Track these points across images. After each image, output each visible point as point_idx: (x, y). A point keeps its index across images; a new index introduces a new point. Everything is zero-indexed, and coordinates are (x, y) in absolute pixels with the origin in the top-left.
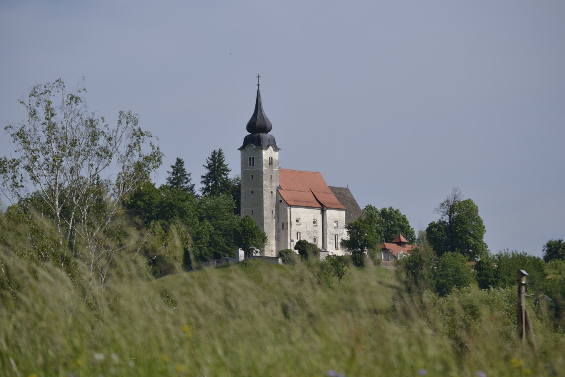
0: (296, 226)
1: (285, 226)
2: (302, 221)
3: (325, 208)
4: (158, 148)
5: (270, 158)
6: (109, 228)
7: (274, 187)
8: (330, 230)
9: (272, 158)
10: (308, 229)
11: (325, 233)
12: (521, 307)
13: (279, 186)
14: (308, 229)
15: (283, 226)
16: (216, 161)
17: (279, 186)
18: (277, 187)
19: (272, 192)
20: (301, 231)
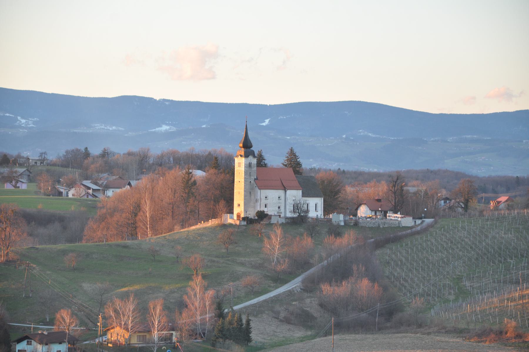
0: (265, 200)
1: (257, 201)
2: (269, 198)
3: (286, 190)
4: (247, 145)
5: (249, 163)
6: (451, 206)
7: (252, 179)
8: (289, 201)
9: (251, 163)
10: (274, 202)
11: (286, 203)
12: (177, 232)
13: (256, 178)
14: (274, 202)
15: (256, 201)
16: (490, 159)
17: (256, 178)
18: (255, 179)
19: (250, 182)
20: (268, 203)
